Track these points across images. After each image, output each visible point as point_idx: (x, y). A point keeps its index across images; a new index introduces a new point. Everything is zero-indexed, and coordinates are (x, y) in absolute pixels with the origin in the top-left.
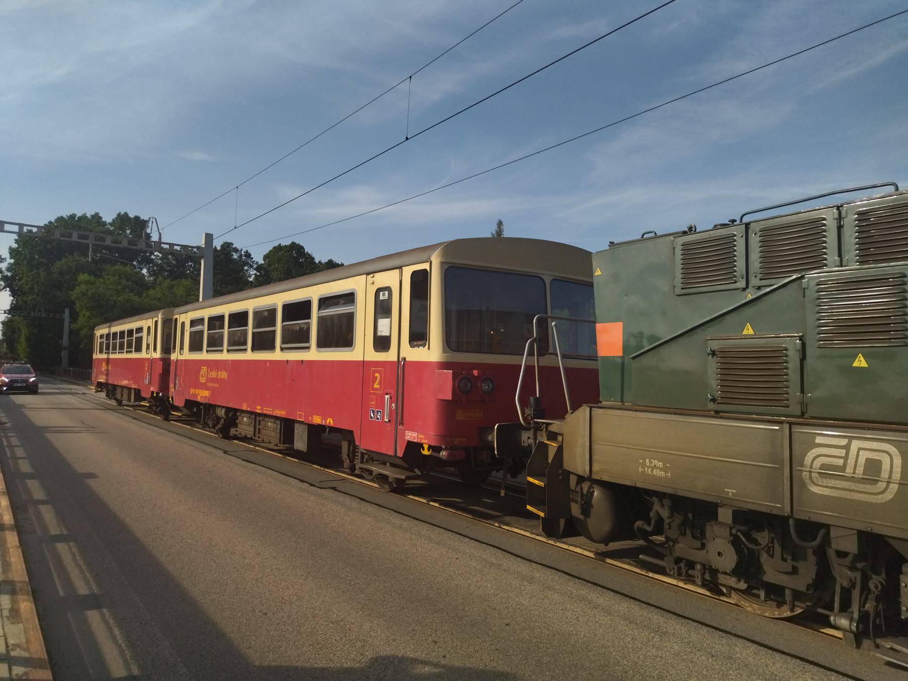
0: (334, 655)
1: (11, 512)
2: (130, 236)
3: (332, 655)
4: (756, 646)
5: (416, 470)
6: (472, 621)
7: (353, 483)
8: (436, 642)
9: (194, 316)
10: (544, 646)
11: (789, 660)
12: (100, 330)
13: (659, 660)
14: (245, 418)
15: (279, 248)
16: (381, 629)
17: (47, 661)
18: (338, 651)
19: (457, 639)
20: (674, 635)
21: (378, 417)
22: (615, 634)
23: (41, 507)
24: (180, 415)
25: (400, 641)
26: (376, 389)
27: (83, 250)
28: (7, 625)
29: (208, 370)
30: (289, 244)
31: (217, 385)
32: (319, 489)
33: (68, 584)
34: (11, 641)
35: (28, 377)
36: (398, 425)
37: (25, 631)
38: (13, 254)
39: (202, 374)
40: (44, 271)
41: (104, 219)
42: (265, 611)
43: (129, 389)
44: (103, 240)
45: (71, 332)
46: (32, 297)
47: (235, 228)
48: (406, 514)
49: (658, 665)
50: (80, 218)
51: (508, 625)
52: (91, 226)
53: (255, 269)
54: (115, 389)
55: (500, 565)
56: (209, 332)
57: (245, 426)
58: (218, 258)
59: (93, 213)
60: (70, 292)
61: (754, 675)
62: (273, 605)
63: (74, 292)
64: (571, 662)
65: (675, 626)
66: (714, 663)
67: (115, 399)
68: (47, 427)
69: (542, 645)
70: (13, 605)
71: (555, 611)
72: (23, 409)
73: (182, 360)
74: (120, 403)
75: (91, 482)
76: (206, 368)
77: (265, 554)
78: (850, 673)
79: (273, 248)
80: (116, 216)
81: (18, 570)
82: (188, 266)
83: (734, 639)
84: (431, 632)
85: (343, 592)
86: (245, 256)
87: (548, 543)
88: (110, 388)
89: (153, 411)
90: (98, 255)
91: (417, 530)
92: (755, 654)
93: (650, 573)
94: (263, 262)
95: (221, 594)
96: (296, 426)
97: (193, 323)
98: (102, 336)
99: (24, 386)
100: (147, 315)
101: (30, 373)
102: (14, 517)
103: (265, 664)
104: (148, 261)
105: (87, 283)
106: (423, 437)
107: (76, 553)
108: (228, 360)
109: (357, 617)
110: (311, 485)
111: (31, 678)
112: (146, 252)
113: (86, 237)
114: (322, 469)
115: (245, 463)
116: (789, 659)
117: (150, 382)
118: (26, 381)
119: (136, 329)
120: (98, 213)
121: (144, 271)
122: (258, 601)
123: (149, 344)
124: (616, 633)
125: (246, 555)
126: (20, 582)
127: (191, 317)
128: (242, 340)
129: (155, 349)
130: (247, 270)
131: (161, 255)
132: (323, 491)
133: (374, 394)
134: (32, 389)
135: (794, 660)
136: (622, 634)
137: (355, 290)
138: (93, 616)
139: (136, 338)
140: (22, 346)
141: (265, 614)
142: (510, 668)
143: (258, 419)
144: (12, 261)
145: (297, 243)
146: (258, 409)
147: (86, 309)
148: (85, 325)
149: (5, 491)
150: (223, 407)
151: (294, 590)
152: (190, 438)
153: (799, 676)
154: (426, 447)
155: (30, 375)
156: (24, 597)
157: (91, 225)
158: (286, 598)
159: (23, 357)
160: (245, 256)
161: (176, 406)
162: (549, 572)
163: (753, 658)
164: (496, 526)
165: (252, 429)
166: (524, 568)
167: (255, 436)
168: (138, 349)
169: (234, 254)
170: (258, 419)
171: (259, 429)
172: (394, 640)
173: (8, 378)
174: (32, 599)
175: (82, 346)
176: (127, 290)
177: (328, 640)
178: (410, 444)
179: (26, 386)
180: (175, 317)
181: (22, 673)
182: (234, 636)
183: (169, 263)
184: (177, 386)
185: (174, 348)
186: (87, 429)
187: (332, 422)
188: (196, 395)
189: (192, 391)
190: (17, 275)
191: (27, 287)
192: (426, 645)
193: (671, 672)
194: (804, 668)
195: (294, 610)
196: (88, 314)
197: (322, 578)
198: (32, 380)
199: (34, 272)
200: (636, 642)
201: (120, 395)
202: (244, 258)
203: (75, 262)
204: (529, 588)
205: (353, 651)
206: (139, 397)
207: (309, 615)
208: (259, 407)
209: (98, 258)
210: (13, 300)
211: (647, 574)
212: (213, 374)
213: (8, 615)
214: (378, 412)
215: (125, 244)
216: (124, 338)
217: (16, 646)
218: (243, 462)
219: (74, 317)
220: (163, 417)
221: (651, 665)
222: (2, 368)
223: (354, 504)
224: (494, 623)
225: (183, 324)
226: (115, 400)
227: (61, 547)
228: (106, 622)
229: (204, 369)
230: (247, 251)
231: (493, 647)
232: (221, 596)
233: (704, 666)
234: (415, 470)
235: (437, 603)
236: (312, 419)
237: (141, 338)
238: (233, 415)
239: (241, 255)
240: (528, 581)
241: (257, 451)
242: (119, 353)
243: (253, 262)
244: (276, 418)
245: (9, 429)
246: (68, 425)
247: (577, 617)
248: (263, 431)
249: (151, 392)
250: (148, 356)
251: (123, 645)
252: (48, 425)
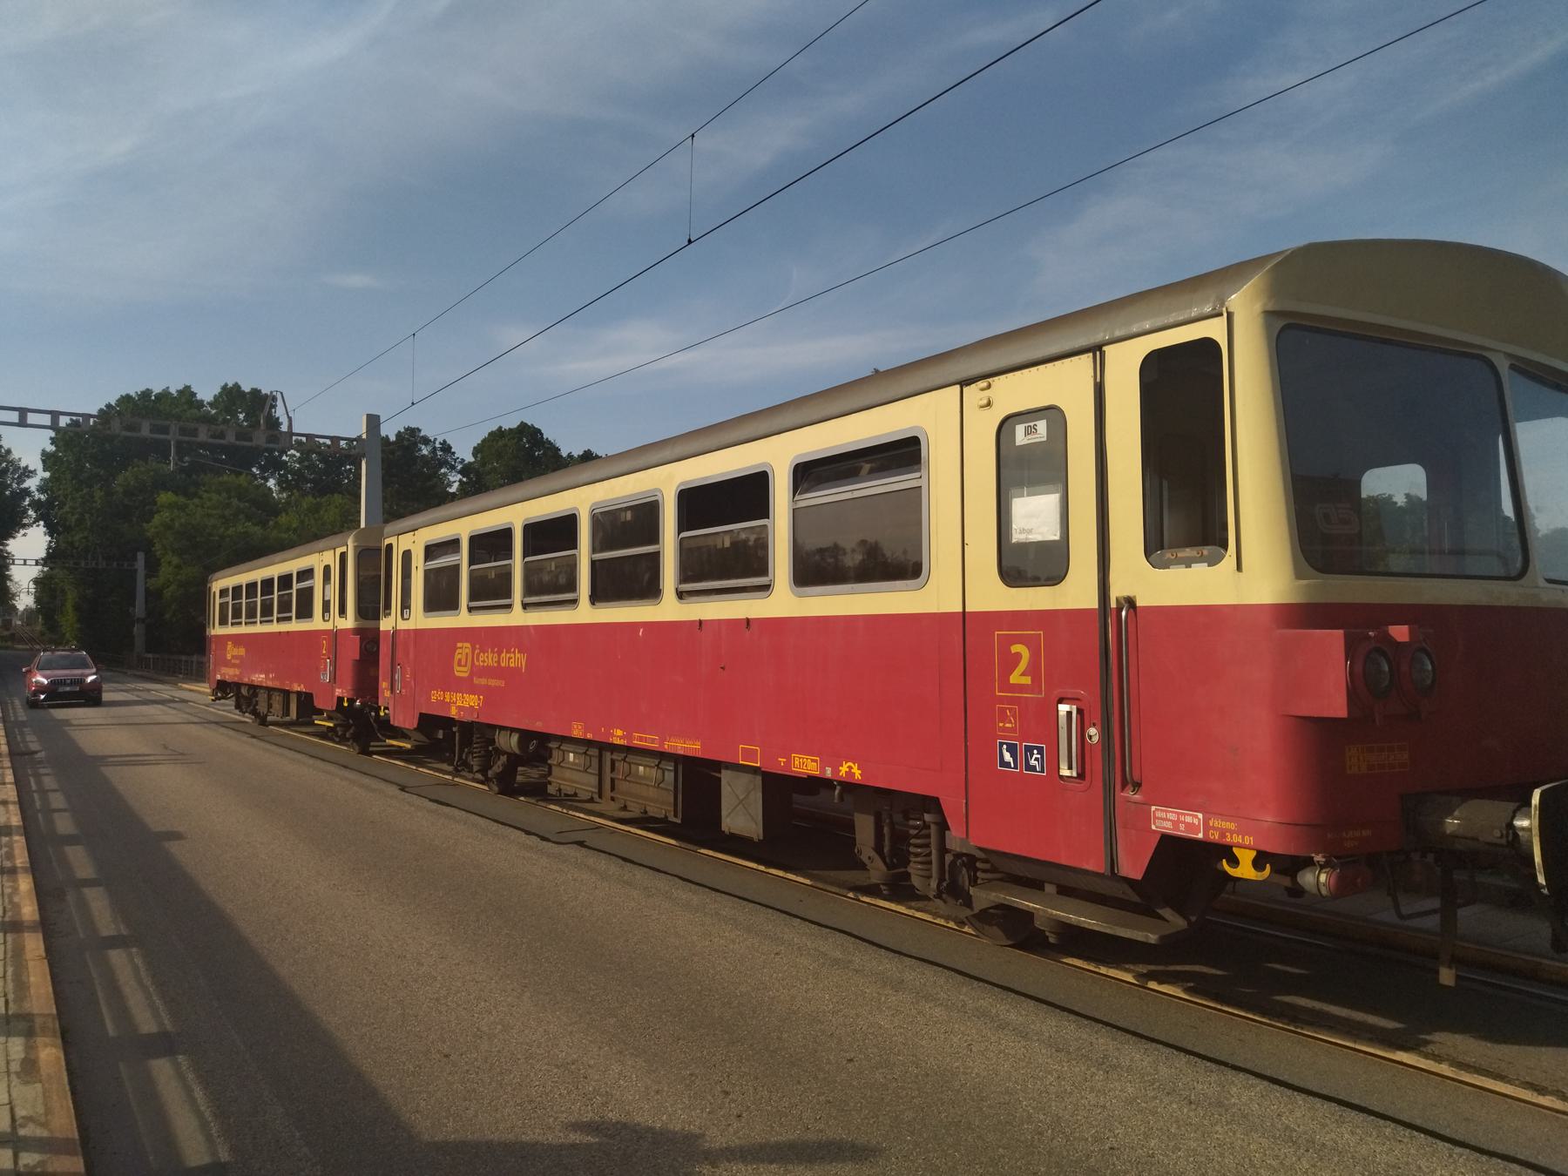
0: (556, 1119)
1: (35, 901)
2: (245, 424)
3: (551, 1120)
4: (1266, 1083)
5: (1167, 913)
6: (791, 1056)
7: (614, 832)
8: (727, 1093)
9: (301, 566)
10: (907, 1094)
11: (1319, 1105)
12: (219, 581)
13: (1098, 1112)
14: (571, 755)
15: (498, 435)
16: (638, 1074)
17: (78, 1142)
18: (563, 1112)
19: (763, 1086)
20: (1129, 1069)
21: (1033, 762)
22: (1029, 1071)
23: (86, 891)
24: (331, 725)
25: (668, 1092)
26: (1021, 688)
27: (162, 450)
28: (15, 1086)
29: (473, 649)
30: (515, 426)
31: (500, 683)
32: (556, 846)
33: (123, 1014)
34: (20, 1112)
35: (82, 675)
36: (1118, 787)
37: (46, 1095)
38: (48, 462)
39: (460, 660)
40: (101, 489)
41: (199, 397)
42: (446, 1051)
43: (286, 694)
44: (194, 432)
45: (148, 593)
46: (81, 535)
47: (413, 404)
48: (741, 895)
49: (1096, 1120)
50: (159, 396)
51: (851, 1060)
52: (177, 410)
53: (460, 472)
54: (255, 695)
55: (850, 962)
56: (473, 567)
57: (570, 769)
58: (391, 456)
59: (181, 387)
60: (145, 525)
61: (1257, 1131)
62: (461, 1040)
63: (151, 524)
64: (950, 1120)
65: (1135, 1055)
66: (1192, 1114)
67: (255, 713)
68: (104, 757)
69: (904, 1092)
70: (27, 1053)
71: (934, 1035)
72: (67, 728)
73: (408, 631)
74: (263, 722)
75: (174, 847)
76: (468, 645)
77: (454, 957)
78: (1418, 1122)
79: (490, 434)
80: (219, 390)
81: (41, 997)
82: (345, 470)
83: (1230, 1073)
84: (722, 1076)
85: (581, 1016)
86: (442, 449)
87: (935, 924)
88: (244, 691)
89: (337, 736)
90: (187, 458)
91: (715, 908)
92: (1262, 1096)
93: (1102, 967)
94: (472, 460)
95: (375, 1026)
96: (726, 776)
97: (431, 551)
98: (223, 592)
99: (76, 692)
100: (322, 543)
101: (86, 666)
102: (40, 909)
103: (439, 1138)
104: (275, 465)
105: (171, 506)
106: (1231, 826)
107: (140, 965)
108: (528, 626)
109: (599, 1055)
110: (543, 839)
111: (50, 1169)
112: (271, 451)
113: (165, 430)
114: (565, 811)
115: (434, 806)
116: (1318, 1102)
117: (334, 678)
118: (81, 681)
119: (298, 573)
120: (189, 387)
121: (271, 483)
122: (436, 1034)
123: (329, 601)
124: (1031, 1068)
125: (423, 960)
126: (41, 1015)
127: (426, 540)
128: (562, 580)
129: (342, 611)
130: (445, 474)
131: (298, 455)
132: (562, 847)
133: (1012, 701)
134: (90, 697)
135: (1327, 1105)
136: (1041, 1070)
137: (512, 523)
138: (162, 1068)
139: (297, 590)
140: (68, 620)
141: (446, 1056)
142: (847, 1132)
143: (608, 756)
144: (47, 475)
145: (529, 424)
146: (618, 737)
147: (173, 552)
148: (171, 579)
149: (28, 865)
150: (513, 730)
151: (498, 1016)
152: (345, 767)
153: (1332, 1130)
154: (1246, 857)
155: (87, 671)
156: (47, 1040)
157: (177, 407)
158: (485, 1029)
159: (71, 639)
160: (442, 449)
161: (397, 727)
162: (930, 971)
163: (1258, 1104)
164: (851, 898)
165: (594, 780)
166: (888, 965)
167: (600, 797)
168: (305, 612)
169: (423, 447)
170: (608, 756)
171: (613, 780)
172: (657, 1092)
173: (47, 678)
174: (59, 1041)
175: (167, 616)
176: (241, 516)
177: (547, 1094)
178: (1170, 845)
179: (80, 691)
180: (387, 541)
181: (35, 1163)
182: (393, 1093)
183: (312, 467)
184: (398, 685)
185: (388, 606)
186: (173, 757)
187: (857, 773)
188: (447, 705)
189: (436, 696)
190: (55, 499)
191: (74, 519)
192: (710, 1098)
193: (1117, 1132)
194: (1341, 1116)
195: (496, 1047)
196: (176, 560)
197: (547, 994)
198: (90, 679)
199: (84, 492)
200: (1063, 1083)
201: (266, 705)
202: (439, 453)
203: (152, 473)
204: (894, 998)
205: (588, 1112)
206: (307, 705)
207: (519, 1056)
208: (619, 733)
209: (187, 464)
210: (50, 542)
211: (1097, 970)
212: (488, 659)
213: (19, 1070)
214: (1029, 750)
215: (230, 438)
216: (273, 594)
217: (30, 1119)
218: (431, 803)
219: (153, 567)
220: (357, 748)
221: (1083, 1121)
222: (37, 660)
223: (613, 867)
224: (828, 1059)
225: (407, 555)
226: (253, 715)
227: (117, 957)
228: (181, 1077)
229: (464, 649)
230: (444, 441)
231: (822, 1098)
232: (375, 1028)
233: (1173, 1119)
234: (1160, 912)
235: (735, 1028)
236: (788, 763)
237: (310, 590)
238: (538, 747)
239: (435, 448)
240: (892, 988)
241: (457, 785)
242: (261, 622)
243: (455, 460)
244: (662, 756)
245: (40, 762)
246: (140, 752)
247: (969, 1045)
248: (622, 786)
249: (335, 701)
250: (328, 626)
251: (207, 1114)
252: (107, 752)
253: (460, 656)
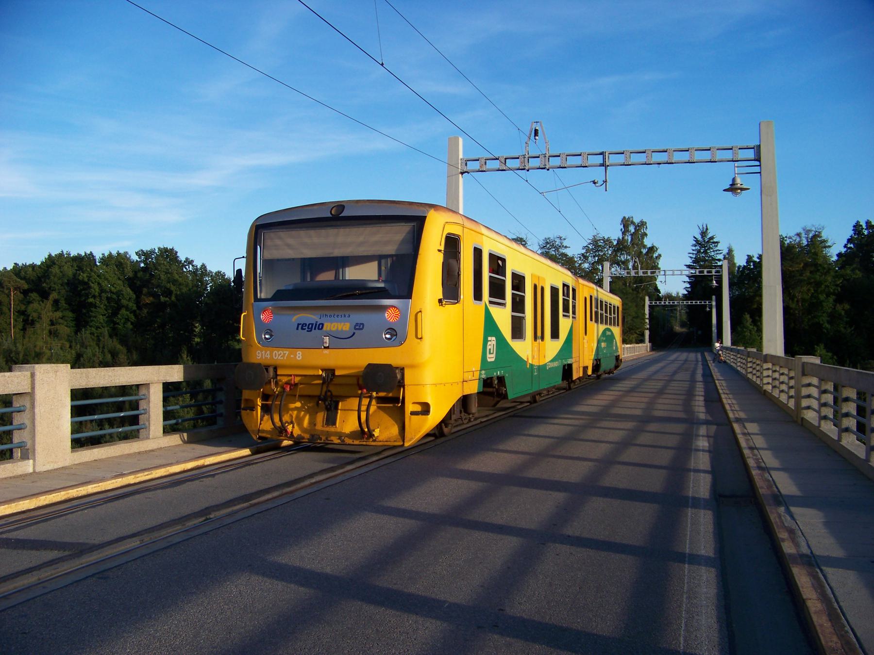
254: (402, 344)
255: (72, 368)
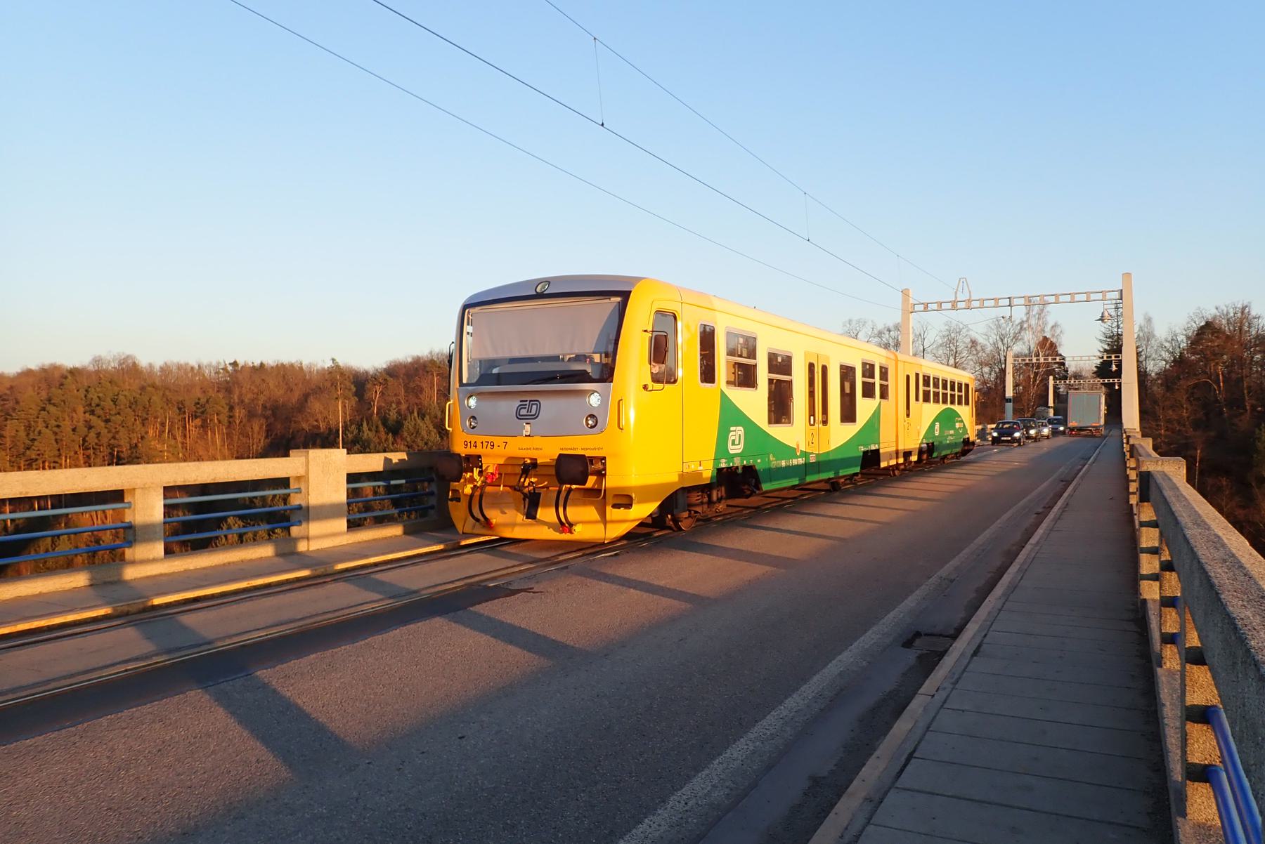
253: (733, 438)
254: (602, 432)
255: (348, 453)
